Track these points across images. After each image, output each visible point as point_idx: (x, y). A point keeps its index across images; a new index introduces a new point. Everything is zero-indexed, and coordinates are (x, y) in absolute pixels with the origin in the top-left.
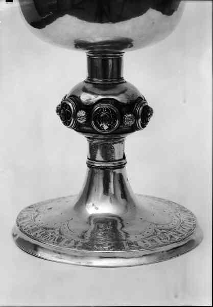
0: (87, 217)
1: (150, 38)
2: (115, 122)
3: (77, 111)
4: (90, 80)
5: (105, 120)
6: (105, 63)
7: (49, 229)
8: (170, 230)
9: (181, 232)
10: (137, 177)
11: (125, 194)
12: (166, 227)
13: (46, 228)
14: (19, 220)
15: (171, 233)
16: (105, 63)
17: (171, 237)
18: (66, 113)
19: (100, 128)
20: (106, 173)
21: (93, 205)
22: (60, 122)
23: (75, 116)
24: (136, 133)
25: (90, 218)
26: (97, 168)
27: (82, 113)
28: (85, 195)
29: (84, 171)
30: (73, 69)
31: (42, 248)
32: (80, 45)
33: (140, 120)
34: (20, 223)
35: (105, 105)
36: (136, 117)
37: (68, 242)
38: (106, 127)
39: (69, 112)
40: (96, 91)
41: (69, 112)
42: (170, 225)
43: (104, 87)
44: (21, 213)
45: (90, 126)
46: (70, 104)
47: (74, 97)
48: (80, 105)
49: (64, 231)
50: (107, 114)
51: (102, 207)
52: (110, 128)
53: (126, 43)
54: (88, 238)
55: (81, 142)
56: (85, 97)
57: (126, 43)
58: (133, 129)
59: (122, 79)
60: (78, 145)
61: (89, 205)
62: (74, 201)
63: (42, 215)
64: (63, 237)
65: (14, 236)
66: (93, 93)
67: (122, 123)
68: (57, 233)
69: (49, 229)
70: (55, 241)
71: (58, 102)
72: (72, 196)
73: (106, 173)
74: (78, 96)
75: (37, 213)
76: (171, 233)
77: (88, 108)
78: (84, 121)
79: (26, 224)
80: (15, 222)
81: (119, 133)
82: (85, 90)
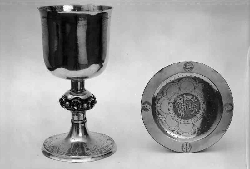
0: (71, 143)
1: (93, 75)
2: (80, 107)
3: (66, 102)
4: (72, 90)
5: (76, 106)
6: (77, 85)
7: (55, 147)
8: (101, 148)
9: (106, 149)
10: (89, 126)
11: (85, 133)
12: (100, 147)
13: (53, 147)
14: (45, 143)
15: (101, 150)
16: (77, 85)
17: (101, 151)
18: (62, 103)
19: (74, 109)
20: (78, 126)
21: (73, 138)
22: (60, 106)
23: (65, 104)
24: (89, 110)
25: (72, 143)
26: (74, 123)
27: (67, 103)
28: (70, 135)
29: (70, 125)
30: (67, 85)
31: (52, 155)
32: (68, 78)
33: (90, 106)
34: (45, 144)
35: (76, 100)
36: (88, 105)
37: (61, 153)
38: (76, 109)
39: (64, 102)
40: (74, 94)
41: (64, 102)
42: (102, 146)
43: (77, 93)
44: (46, 140)
45: (70, 107)
46: (63, 99)
47: (65, 97)
48: (67, 100)
49: (60, 148)
50: (78, 103)
51: (77, 139)
52: (78, 109)
53: (83, 79)
54: (71, 151)
55: (69, 113)
56: (70, 97)
57: (86, 77)
58: (87, 109)
59: (84, 89)
60: (67, 115)
61: (72, 138)
62: (67, 135)
63: (53, 141)
64: (59, 150)
65: (42, 149)
66: (73, 95)
67: (83, 106)
68: (57, 149)
69: (55, 147)
70: (56, 152)
71: (60, 97)
72: (65, 133)
73: (78, 126)
74: (67, 96)
75: (52, 140)
76: (101, 150)
77: (70, 101)
78: (68, 106)
79: (48, 145)
80: (43, 143)
81: (83, 111)
82: (70, 94)
